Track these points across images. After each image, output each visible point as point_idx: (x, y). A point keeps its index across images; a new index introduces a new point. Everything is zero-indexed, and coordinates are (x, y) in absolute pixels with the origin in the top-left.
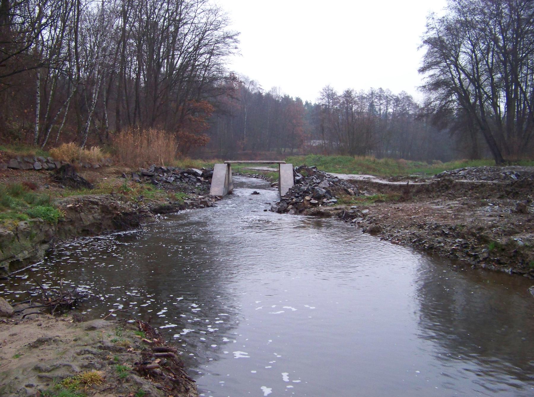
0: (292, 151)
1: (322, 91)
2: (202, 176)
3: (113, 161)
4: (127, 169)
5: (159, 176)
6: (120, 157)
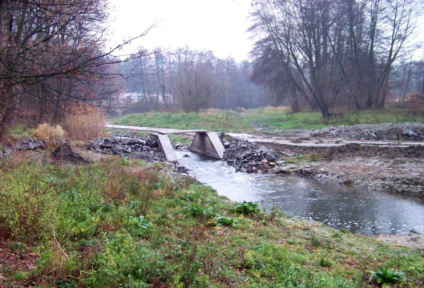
2: (147, 144)
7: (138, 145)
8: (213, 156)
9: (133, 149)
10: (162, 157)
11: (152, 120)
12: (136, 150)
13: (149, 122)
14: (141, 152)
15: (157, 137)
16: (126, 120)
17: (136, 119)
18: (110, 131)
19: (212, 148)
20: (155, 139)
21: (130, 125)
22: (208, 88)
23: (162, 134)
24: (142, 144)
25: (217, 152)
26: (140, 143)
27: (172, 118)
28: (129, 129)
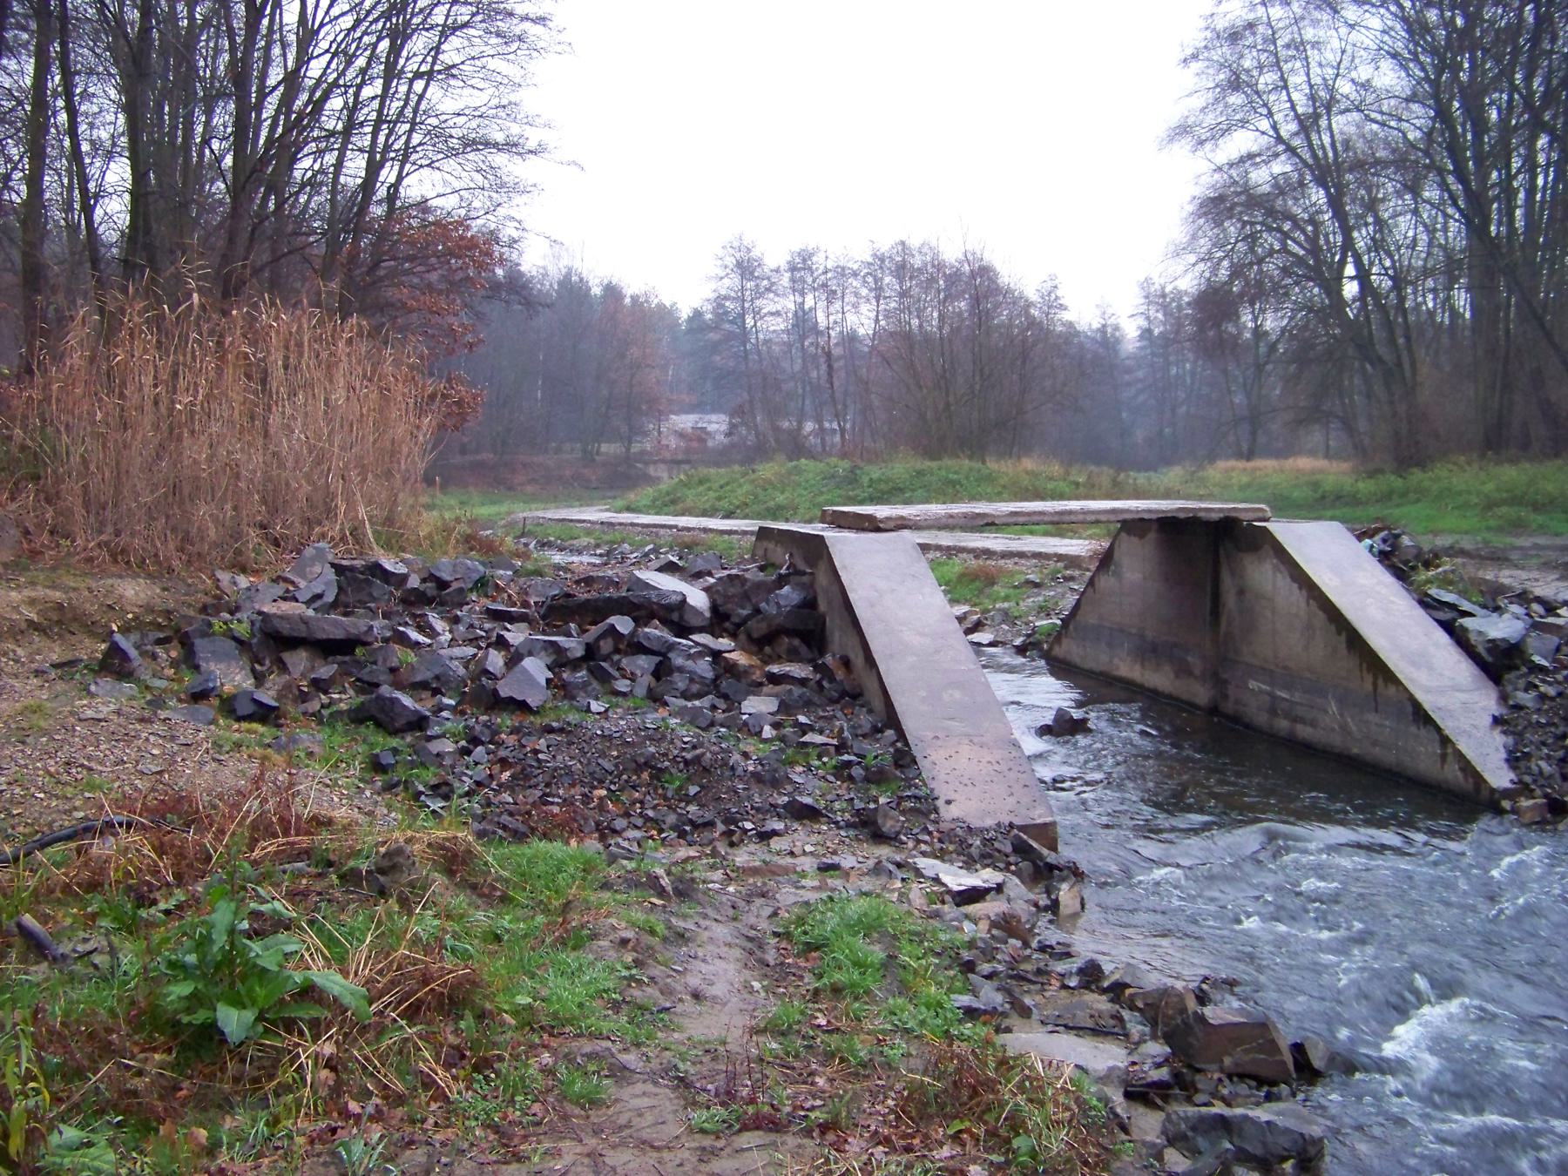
0: (628, 449)
1: (721, 253)
2: (719, 620)
3: (15, 532)
4: (134, 591)
5: (403, 639)
6: (73, 501)
7: (623, 624)
8: (1378, 754)
9: (575, 664)
10: (877, 777)
11: (774, 488)
12: (604, 677)
13: (761, 497)
14: (655, 698)
15: (815, 549)
16: (668, 494)
17: (710, 489)
18: (588, 533)
19: (1347, 664)
20: (795, 572)
21: (683, 514)
22: (1025, 357)
23: (872, 525)
24: (675, 616)
25: (1421, 717)
26: (646, 608)
27: (865, 480)
28: (671, 527)
